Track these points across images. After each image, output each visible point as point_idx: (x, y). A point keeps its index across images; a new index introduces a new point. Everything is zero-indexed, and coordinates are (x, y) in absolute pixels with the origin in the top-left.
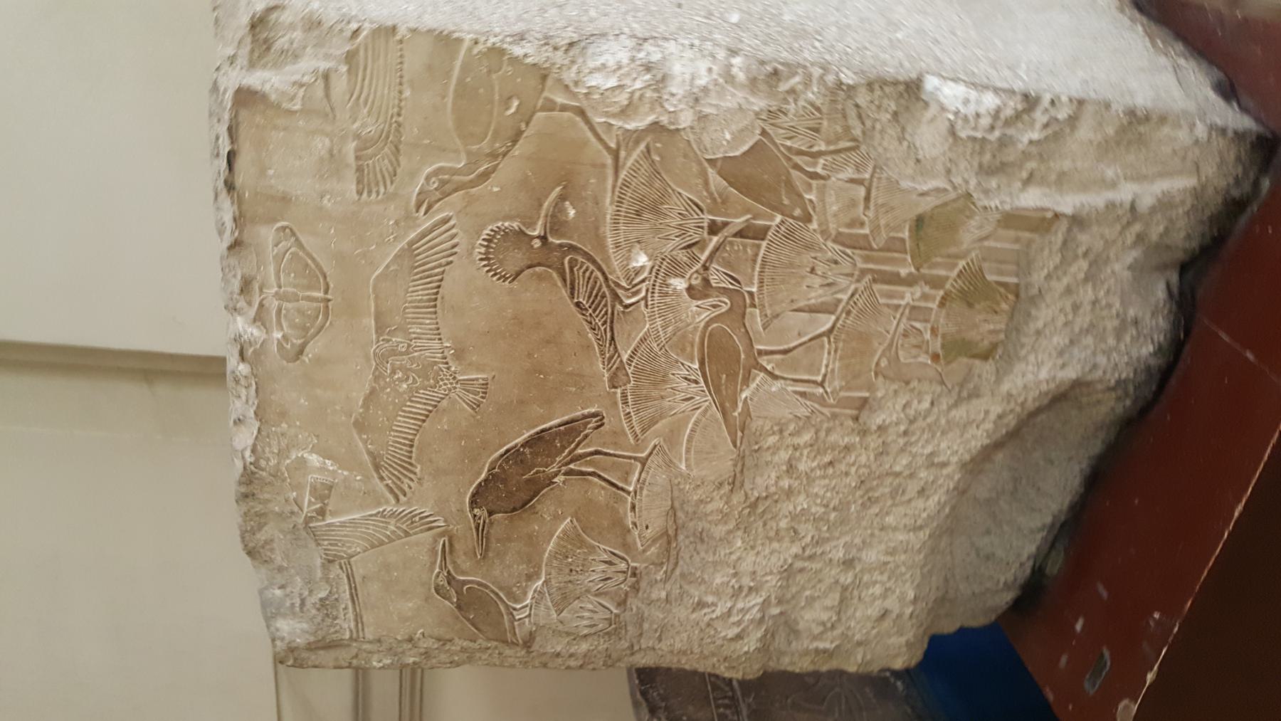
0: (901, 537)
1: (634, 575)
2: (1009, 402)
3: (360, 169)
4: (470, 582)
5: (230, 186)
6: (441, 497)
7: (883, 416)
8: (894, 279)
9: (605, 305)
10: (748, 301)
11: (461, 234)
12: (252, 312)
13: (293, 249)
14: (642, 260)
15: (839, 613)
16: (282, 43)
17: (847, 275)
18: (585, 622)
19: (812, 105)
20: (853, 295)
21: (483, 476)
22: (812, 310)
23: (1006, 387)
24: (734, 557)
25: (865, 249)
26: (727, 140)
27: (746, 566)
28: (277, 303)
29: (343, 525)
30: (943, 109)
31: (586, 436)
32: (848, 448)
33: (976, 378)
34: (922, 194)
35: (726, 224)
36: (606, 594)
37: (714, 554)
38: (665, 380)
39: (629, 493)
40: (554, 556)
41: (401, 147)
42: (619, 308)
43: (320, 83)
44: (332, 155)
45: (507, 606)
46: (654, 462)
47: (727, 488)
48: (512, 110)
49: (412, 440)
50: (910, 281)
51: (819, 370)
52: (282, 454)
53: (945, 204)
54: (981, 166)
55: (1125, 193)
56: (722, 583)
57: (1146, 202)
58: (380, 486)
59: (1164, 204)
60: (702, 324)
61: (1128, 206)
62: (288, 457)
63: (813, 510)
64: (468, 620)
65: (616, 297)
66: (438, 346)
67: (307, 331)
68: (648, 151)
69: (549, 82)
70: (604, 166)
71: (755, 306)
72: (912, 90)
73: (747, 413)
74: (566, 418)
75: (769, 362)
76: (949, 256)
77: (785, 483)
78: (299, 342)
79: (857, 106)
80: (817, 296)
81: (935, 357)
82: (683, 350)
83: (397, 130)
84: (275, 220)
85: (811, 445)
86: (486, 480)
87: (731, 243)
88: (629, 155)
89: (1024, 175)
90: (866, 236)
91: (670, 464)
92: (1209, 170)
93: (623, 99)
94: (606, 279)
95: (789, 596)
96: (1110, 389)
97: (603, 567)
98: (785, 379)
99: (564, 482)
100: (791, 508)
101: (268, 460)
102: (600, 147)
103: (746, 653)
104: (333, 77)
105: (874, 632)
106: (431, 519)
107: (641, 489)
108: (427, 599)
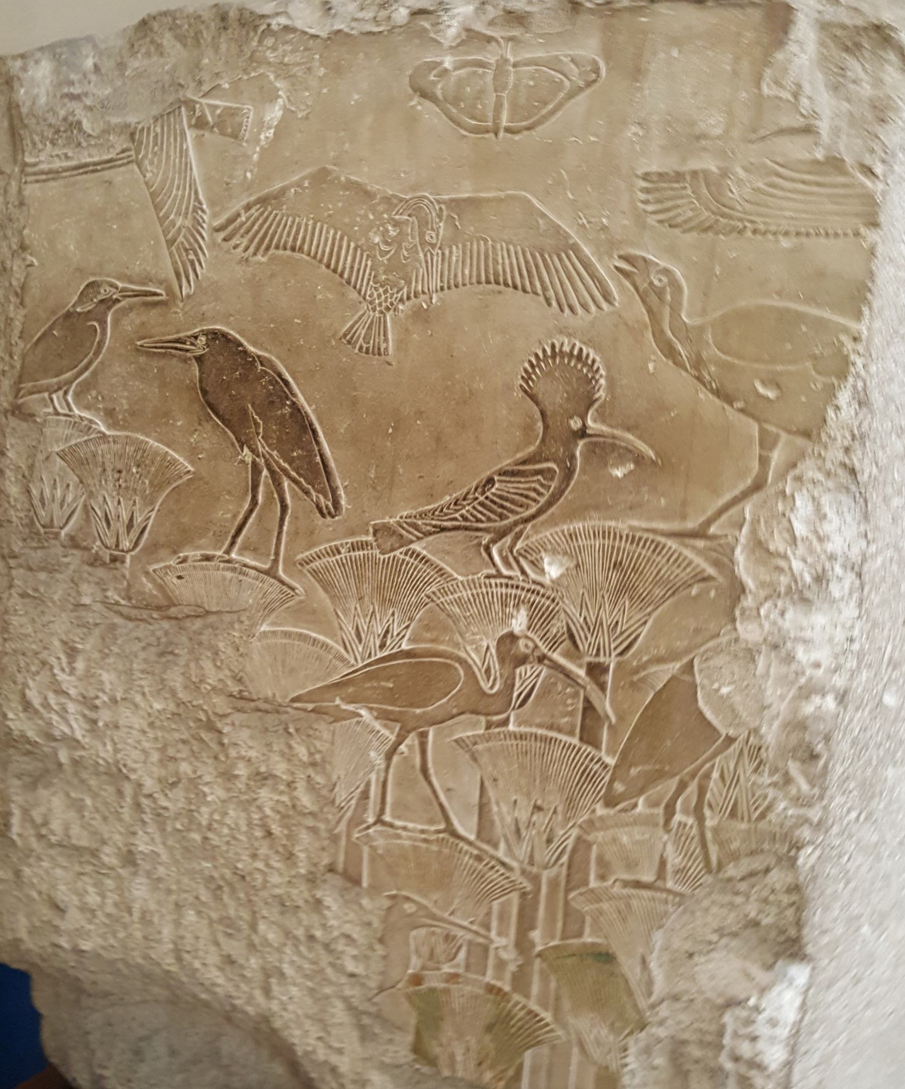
1: (114, 559)
3: (679, 176)
6: (223, 291)
8: (526, 922)
9: (489, 520)
11: (589, 318)
13: (567, 83)
15: (60, 845)
17: (531, 857)
18: (47, 492)
20: (503, 864)
21: (251, 349)
22: (483, 808)
24: (138, 698)
29: (184, 153)
31: (307, 493)
32: (289, 857)
33: (387, 1036)
34: (644, 962)
35: (602, 687)
37: (143, 671)
39: (228, 552)
42: (486, 538)
43: (799, 122)
44: (698, 138)
45: (69, 382)
47: (235, 689)
48: (761, 390)
49: (301, 249)
50: (523, 944)
51: (399, 818)
52: (282, 69)
53: (630, 993)
58: (237, 206)
60: (463, 655)
62: (277, 76)
64: (51, 328)
65: (501, 534)
66: (432, 286)
67: (451, 103)
69: (800, 441)
70: (684, 517)
71: (488, 727)
73: (339, 716)
74: (332, 464)
78: (439, 93)
80: (503, 814)
81: (417, 980)
82: (427, 628)
83: (733, 229)
84: (608, 58)
86: (245, 352)
87: (575, 695)
90: (586, 882)
91: (268, 609)
93: (778, 543)
97: (125, 517)
99: (242, 462)
100: (207, 778)
101: (274, 49)
102: (710, 513)
107: (234, 570)
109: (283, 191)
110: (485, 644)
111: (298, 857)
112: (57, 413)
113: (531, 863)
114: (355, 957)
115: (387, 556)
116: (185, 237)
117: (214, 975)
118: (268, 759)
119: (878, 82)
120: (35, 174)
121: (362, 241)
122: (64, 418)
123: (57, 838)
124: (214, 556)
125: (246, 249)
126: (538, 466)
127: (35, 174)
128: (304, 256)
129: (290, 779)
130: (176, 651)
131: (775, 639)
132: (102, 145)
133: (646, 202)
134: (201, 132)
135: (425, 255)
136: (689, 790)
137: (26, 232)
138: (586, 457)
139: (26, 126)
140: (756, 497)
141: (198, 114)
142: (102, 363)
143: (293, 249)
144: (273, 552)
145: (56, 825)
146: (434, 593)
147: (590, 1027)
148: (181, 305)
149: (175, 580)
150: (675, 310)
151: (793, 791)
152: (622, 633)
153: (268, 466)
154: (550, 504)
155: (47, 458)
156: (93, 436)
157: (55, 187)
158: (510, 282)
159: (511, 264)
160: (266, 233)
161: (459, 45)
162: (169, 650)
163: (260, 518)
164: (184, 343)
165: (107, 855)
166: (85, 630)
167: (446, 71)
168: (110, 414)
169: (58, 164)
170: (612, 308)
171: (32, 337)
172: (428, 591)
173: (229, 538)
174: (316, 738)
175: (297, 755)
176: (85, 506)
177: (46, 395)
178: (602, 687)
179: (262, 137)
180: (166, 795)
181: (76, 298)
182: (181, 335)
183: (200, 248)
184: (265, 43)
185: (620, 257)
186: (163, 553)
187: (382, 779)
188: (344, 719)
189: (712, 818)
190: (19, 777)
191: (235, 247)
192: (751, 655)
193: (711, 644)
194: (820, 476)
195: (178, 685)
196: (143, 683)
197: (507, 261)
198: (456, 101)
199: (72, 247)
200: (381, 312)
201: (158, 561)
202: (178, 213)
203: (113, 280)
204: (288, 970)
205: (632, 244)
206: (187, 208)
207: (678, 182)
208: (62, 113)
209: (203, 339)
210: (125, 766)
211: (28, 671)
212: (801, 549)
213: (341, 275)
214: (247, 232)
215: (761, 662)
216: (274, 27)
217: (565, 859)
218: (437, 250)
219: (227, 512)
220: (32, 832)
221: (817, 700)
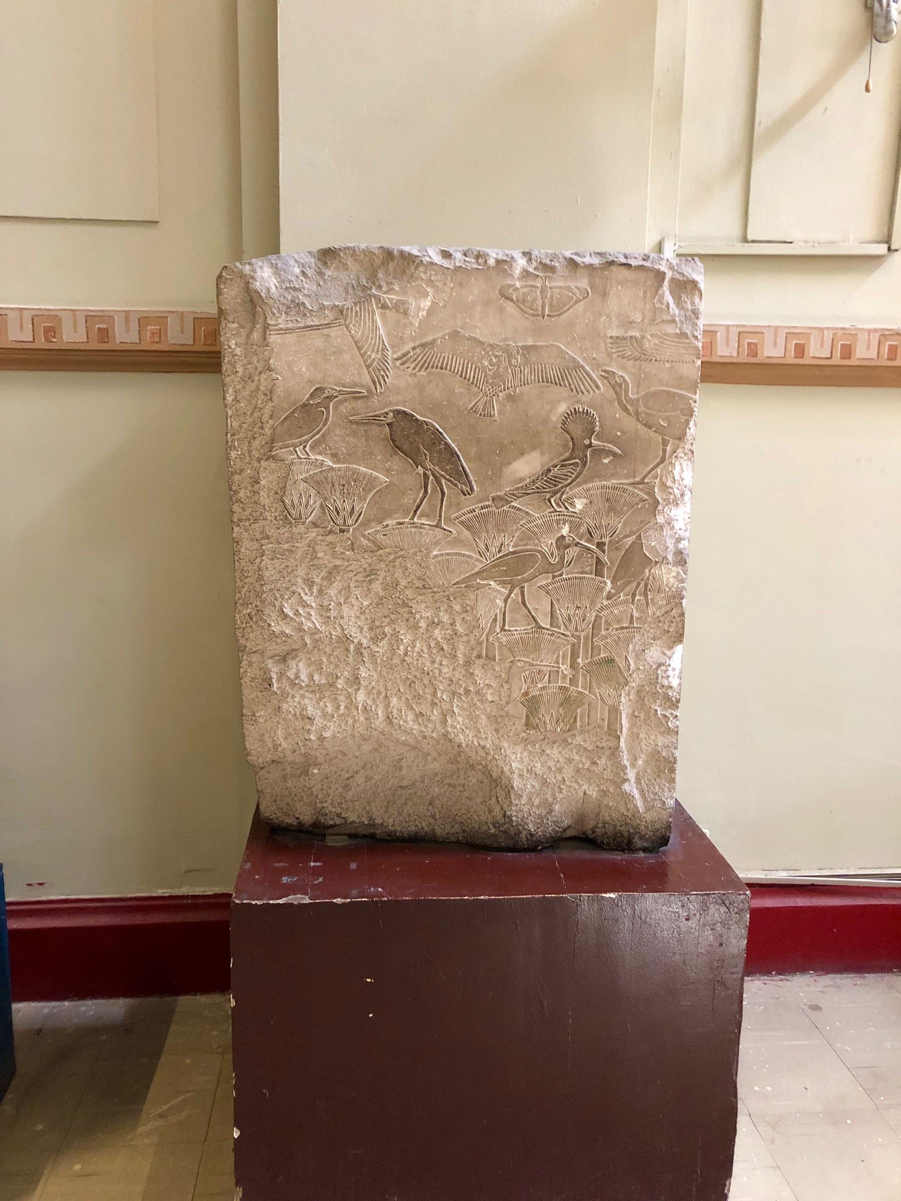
3: (624, 338)
5: (612, 263)
6: (401, 390)
8: (574, 655)
9: (550, 487)
17: (576, 628)
18: (296, 501)
20: (564, 634)
21: (419, 417)
31: (456, 485)
35: (604, 552)
36: (324, 513)
37: (355, 587)
39: (412, 519)
43: (670, 318)
44: (631, 323)
49: (446, 368)
52: (430, 282)
55: (631, 774)
57: (626, 787)
58: (408, 347)
59: (627, 798)
60: (540, 549)
64: (293, 412)
65: (555, 493)
69: (677, 442)
70: (634, 477)
71: (554, 577)
72: (679, 638)
74: (468, 470)
80: (561, 612)
81: (526, 694)
82: (521, 540)
86: (417, 420)
91: (437, 543)
92: (649, 817)
93: (669, 483)
94: (567, 486)
97: (349, 509)
101: (425, 273)
103: (269, 625)
109: (434, 341)
113: (576, 630)
119: (693, 303)
120: (277, 330)
125: (414, 369)
127: (277, 330)
137: (271, 361)
140: (662, 466)
141: (382, 302)
142: (328, 429)
143: (441, 368)
147: (606, 691)
154: (577, 477)
157: (290, 338)
163: (429, 500)
167: (517, 289)
168: (335, 457)
169: (290, 325)
172: (521, 523)
176: (321, 505)
177: (292, 449)
178: (604, 552)
181: (308, 396)
186: (373, 524)
190: (271, 658)
191: (408, 368)
192: (662, 527)
194: (682, 455)
198: (523, 302)
201: (370, 528)
202: (373, 351)
205: (606, 365)
208: (290, 298)
209: (392, 414)
212: (677, 485)
213: (469, 380)
214: (415, 360)
215: (665, 529)
216: (424, 262)
217: (591, 626)
219: (409, 500)
221: (682, 542)
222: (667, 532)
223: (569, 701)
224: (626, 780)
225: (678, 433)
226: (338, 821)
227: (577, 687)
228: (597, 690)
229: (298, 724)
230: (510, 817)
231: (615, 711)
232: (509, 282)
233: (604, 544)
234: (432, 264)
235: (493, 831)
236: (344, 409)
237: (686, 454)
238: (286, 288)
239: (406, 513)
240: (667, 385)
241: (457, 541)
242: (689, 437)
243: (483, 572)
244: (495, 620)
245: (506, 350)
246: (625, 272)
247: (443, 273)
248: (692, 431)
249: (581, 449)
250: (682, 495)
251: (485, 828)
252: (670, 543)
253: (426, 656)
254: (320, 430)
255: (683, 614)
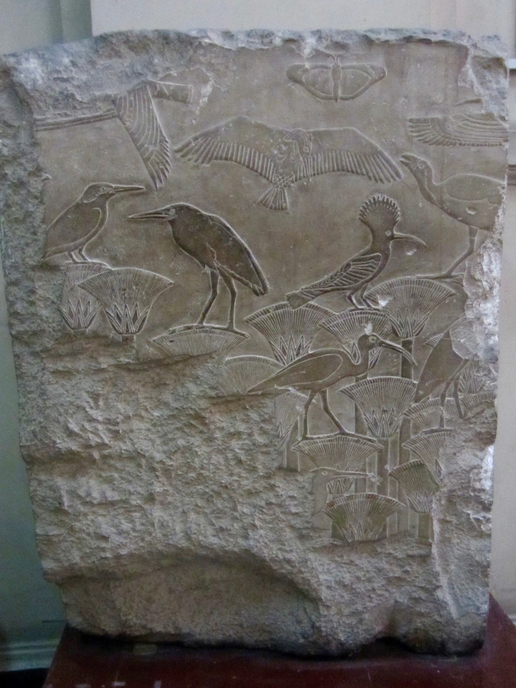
0: (178, 528)
1: (126, 340)
2: (299, 562)
3: (425, 121)
4: (104, 212)
5: (409, 39)
6: (184, 185)
7: (281, 485)
8: (382, 461)
9: (350, 284)
10: (360, 376)
11: (390, 184)
12: (321, 48)
13: (370, 78)
14: (383, 303)
15: (100, 504)
16: (489, 76)
17: (383, 433)
18: (74, 309)
19: (484, 385)
20: (370, 440)
21: (204, 213)
22: (357, 419)
23: (311, 556)
24: (143, 413)
25: (400, 439)
26: (462, 342)
27: (136, 424)
28: (331, 65)
29: (150, 111)
30: (482, 460)
31: (247, 284)
32: (254, 469)
33: (317, 535)
34: (437, 463)
35: (410, 351)
36: (104, 320)
37: (145, 398)
38: (297, 332)
39: (201, 322)
40: (136, 275)
41: (441, 146)
42: (348, 293)
43: (474, 98)
44: (432, 104)
45: (83, 244)
46: (231, 338)
47: (213, 393)
48: (470, 212)
49: (231, 159)
50: (381, 473)
51: (315, 434)
52: (210, 66)
53: (431, 477)
54: (454, 491)
55: (444, 580)
56: (118, 409)
57: (439, 594)
58: (189, 138)
59: (440, 605)
60: (342, 350)
61: (438, 584)
62: (207, 70)
63: (196, 460)
64: (66, 214)
65: (356, 290)
66: (309, 174)
67: (312, 88)
68: (451, 295)
69: (485, 232)
70: (440, 269)
71: (357, 381)
72: (488, 438)
73: (278, 393)
74: (260, 268)
75: (318, 400)
76: (400, 490)
77: (218, 435)
78: (304, 80)
79: (483, 411)
80: (366, 417)
81: (331, 504)
82: (321, 341)
83: (451, 143)
84: (388, 66)
85: (254, 444)
86: (202, 215)
87: (398, 357)
88: (449, 284)
89: (448, 519)
90: (409, 437)
91: (230, 349)
92: (463, 623)
93: (478, 276)
94: (367, 282)
95: (112, 462)
96: (313, 626)
97: (131, 314)
98: (306, 414)
99: (205, 274)
100: (196, 444)
101: (204, 55)
102: (451, 266)
103: (55, 442)
104: (478, 106)
105: (84, 536)
106: (162, 177)
107: (206, 332)
108: (84, 180)
110: (352, 342)
111: (258, 468)
112: (76, 263)
114: (295, 505)
115: (296, 309)
116: (156, 156)
117: (214, 540)
118: (234, 425)
120: (43, 125)
121: (268, 153)
122: (81, 265)
123: (98, 500)
124: (192, 326)
126: (372, 255)
127: (43, 125)
128: (233, 162)
129: (249, 431)
130: (167, 382)
131: (478, 316)
132: (91, 108)
133: (412, 132)
134: (161, 99)
135: (304, 159)
136: (451, 385)
138: (394, 248)
139: (32, 97)
140: (469, 257)
141: (158, 89)
143: (226, 159)
144: (229, 318)
145: (96, 494)
146: (324, 323)
147: (417, 498)
148: (156, 193)
149: (169, 344)
150: (430, 180)
151: (491, 376)
152: (417, 325)
153: (222, 274)
155: (72, 289)
156: (103, 272)
157: (60, 134)
158: (350, 169)
159: (349, 161)
160: (209, 152)
161: (312, 57)
162: (162, 382)
164: (161, 214)
165: (134, 500)
166: (104, 383)
168: (114, 260)
169: (60, 119)
170: (400, 180)
171: (52, 220)
173: (201, 316)
174: (264, 407)
175: (252, 419)
176: (102, 313)
177: (66, 253)
178: (410, 351)
179: (201, 101)
180: (171, 458)
182: (159, 209)
183: (167, 162)
184: (198, 52)
185: (403, 156)
187: (304, 418)
188: (280, 394)
189: (461, 395)
191: (189, 160)
192: (470, 324)
193: (455, 323)
194: (491, 245)
195: (170, 400)
196: (145, 404)
197: (347, 160)
198: (314, 85)
199: (76, 167)
200: (281, 188)
203: (108, 183)
204: (257, 523)
206: (156, 141)
207: (425, 123)
209: (174, 210)
210: (142, 450)
211: (67, 414)
215: (474, 326)
218: (310, 156)
220: (78, 502)
221: (493, 338)
222: (476, 328)
223: (377, 511)
224: (438, 587)
225: (486, 222)
226: (144, 632)
227: (386, 494)
228: (407, 497)
229: (94, 543)
230: (319, 629)
231: (426, 519)
232: (297, 63)
233: (410, 342)
234: (212, 45)
235: (302, 641)
236: (121, 207)
237: (494, 244)
238: (55, 79)
239: (194, 317)
240: (472, 170)
241: (251, 347)
242: (497, 226)
243: (282, 375)
244: (296, 428)
245: (296, 136)
246: (424, 50)
247: (225, 56)
248: (501, 218)
249: (384, 241)
250: (491, 288)
251: (294, 638)
252: (480, 340)
253: (223, 468)
254: (96, 232)
255: (495, 415)
